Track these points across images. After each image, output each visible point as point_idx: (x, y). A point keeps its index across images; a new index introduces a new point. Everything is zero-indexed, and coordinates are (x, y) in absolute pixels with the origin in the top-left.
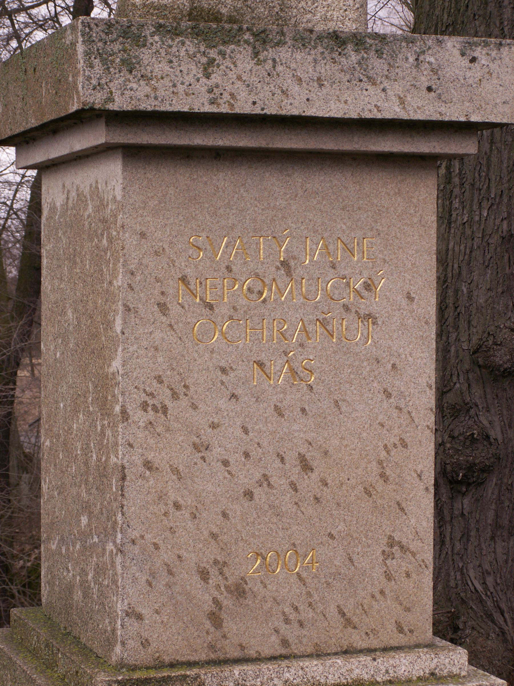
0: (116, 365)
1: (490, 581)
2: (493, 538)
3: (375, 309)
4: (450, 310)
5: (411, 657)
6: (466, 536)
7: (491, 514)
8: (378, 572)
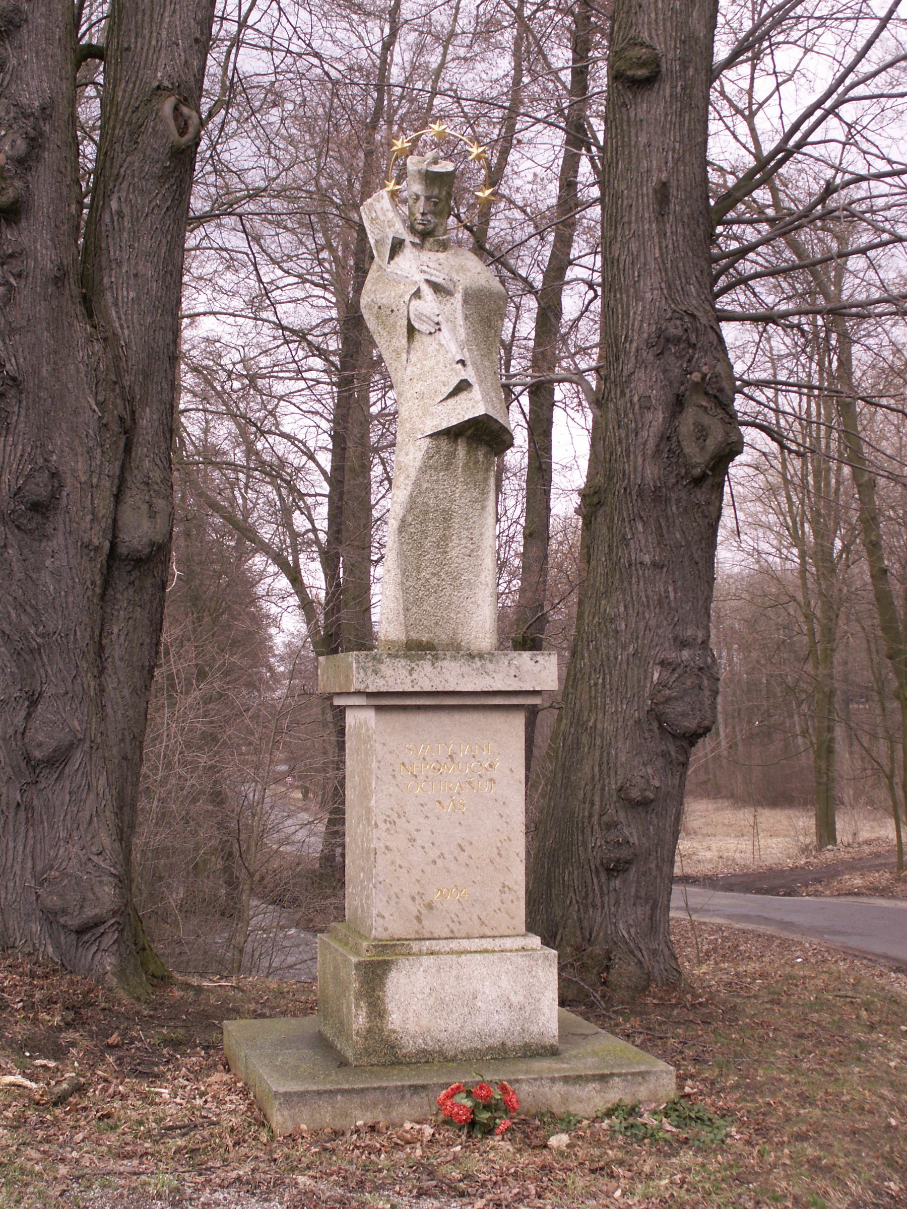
0: (373, 802)
1: (632, 931)
2: (634, 904)
3: (494, 776)
4: (605, 765)
5: (512, 939)
6: (617, 903)
7: (633, 890)
8: (497, 900)
